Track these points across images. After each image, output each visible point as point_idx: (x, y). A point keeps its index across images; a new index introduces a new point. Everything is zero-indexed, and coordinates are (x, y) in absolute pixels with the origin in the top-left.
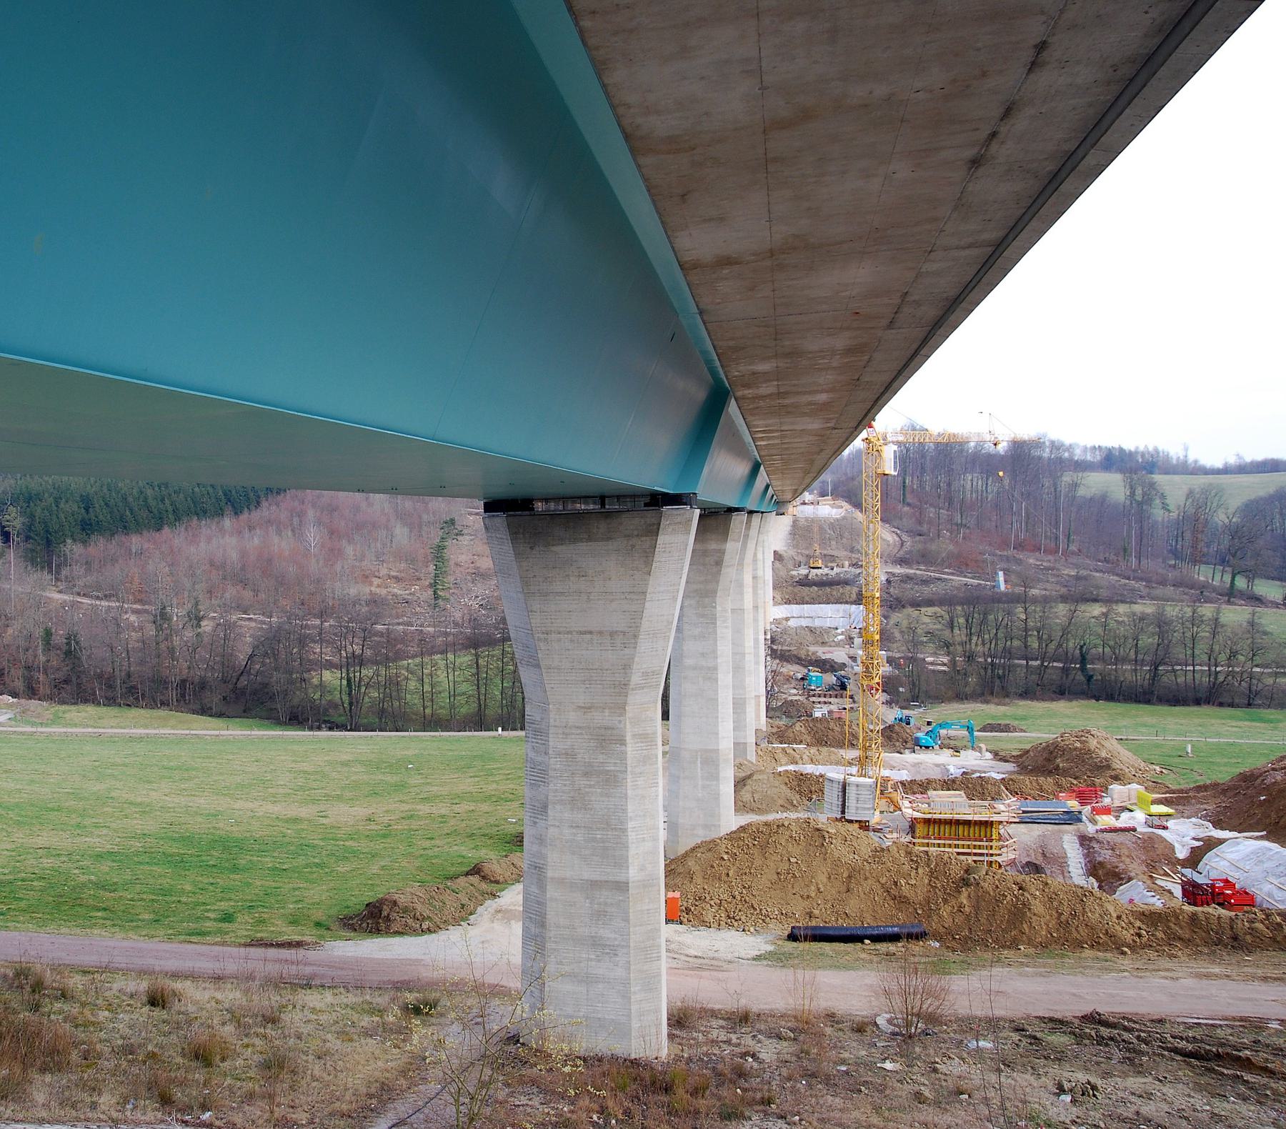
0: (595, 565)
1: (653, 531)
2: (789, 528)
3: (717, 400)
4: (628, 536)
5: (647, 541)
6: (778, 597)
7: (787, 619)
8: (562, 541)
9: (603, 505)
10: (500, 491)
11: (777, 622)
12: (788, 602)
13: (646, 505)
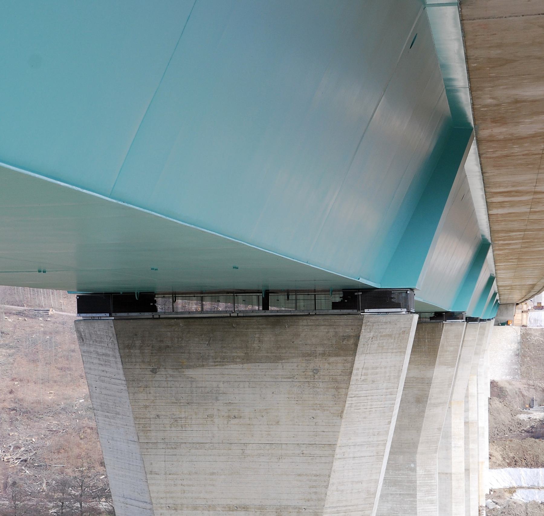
0: (253, 400)
1: (348, 347)
2: (515, 346)
3: (453, 140)
4: (309, 355)
5: (336, 364)
6: (498, 455)
7: (512, 490)
8: (202, 361)
9: (266, 307)
10: (108, 276)
11: (494, 494)
12: (514, 463)
13: (335, 306)
